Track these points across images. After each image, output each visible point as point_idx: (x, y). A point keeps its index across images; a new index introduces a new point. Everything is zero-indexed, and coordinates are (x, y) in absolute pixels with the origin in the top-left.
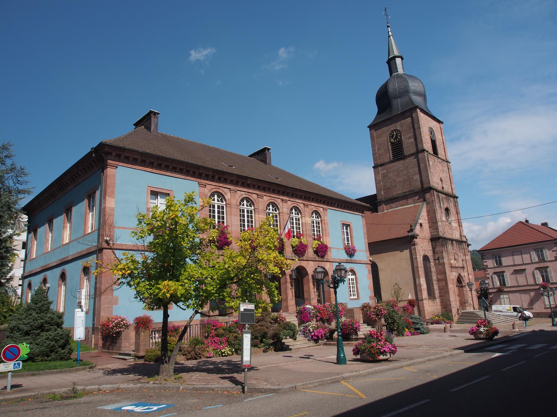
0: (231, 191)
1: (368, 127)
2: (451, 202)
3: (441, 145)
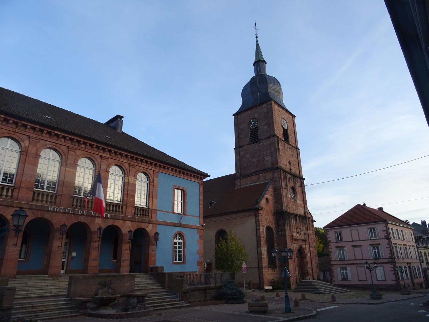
3: (293, 134)
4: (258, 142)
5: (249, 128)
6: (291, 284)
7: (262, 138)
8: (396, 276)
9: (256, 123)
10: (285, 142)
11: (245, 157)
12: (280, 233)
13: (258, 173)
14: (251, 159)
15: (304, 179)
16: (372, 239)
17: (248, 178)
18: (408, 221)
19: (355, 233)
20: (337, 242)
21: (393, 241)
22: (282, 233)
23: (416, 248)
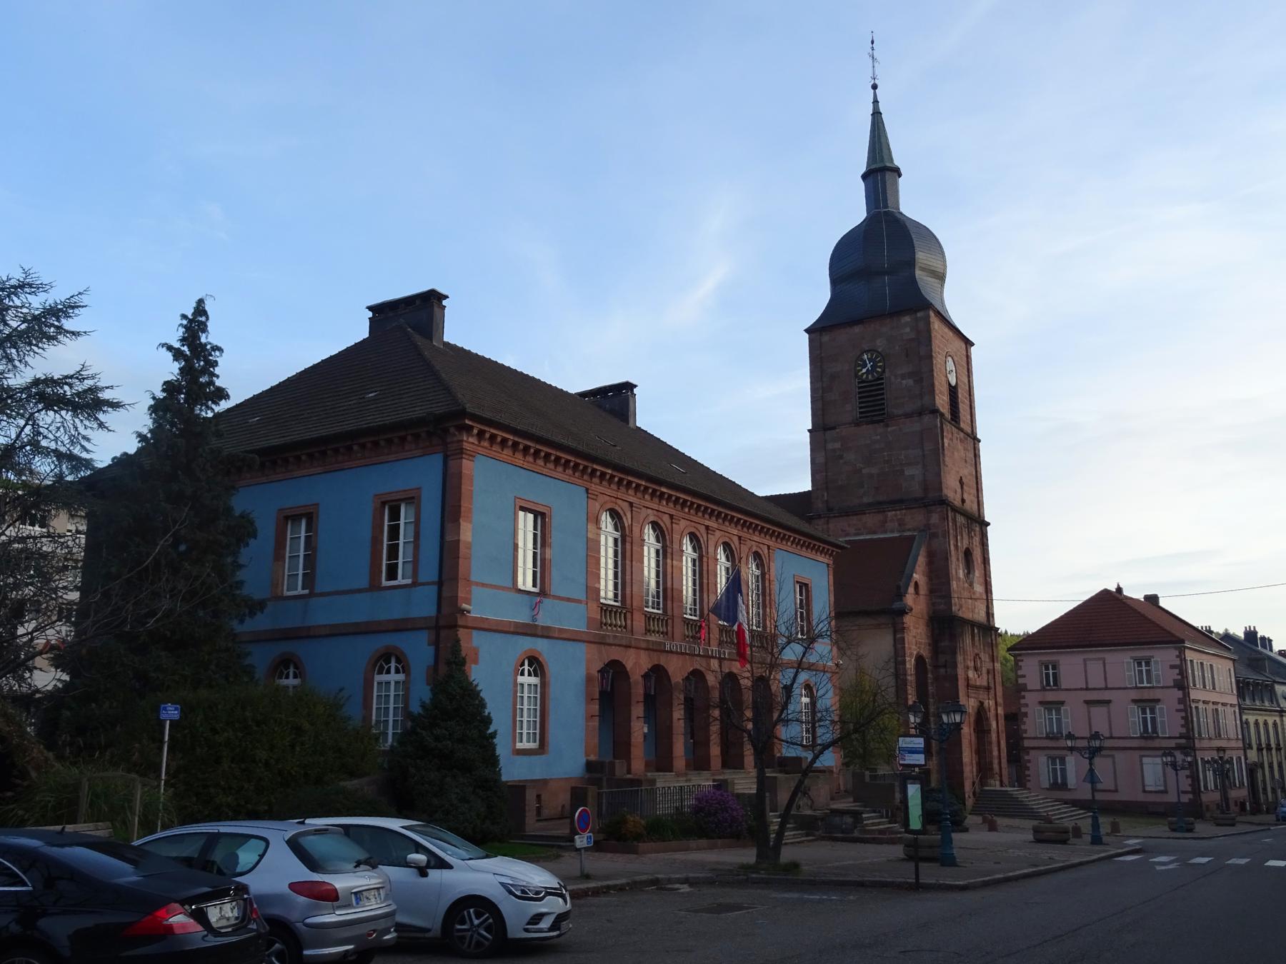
0: (589, 495)
1: (806, 331)
2: (975, 535)
3: (966, 398)
4: (883, 422)
5: (856, 376)
6: (967, 796)
7: (896, 412)
8: (1192, 781)
9: (879, 364)
10: (953, 425)
11: (841, 457)
12: (942, 671)
13: (879, 507)
14: (861, 465)
15: (988, 524)
16: (1138, 685)
17: (851, 517)
18: (1209, 627)
19: (1095, 669)
20: (1043, 689)
21: (1194, 695)
22: (946, 672)
23: (1237, 711)
